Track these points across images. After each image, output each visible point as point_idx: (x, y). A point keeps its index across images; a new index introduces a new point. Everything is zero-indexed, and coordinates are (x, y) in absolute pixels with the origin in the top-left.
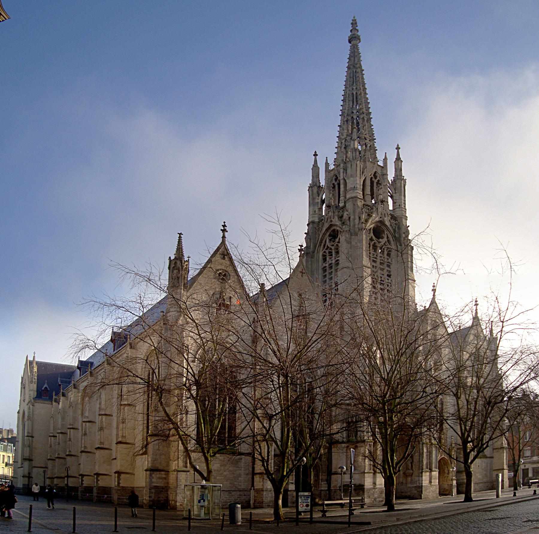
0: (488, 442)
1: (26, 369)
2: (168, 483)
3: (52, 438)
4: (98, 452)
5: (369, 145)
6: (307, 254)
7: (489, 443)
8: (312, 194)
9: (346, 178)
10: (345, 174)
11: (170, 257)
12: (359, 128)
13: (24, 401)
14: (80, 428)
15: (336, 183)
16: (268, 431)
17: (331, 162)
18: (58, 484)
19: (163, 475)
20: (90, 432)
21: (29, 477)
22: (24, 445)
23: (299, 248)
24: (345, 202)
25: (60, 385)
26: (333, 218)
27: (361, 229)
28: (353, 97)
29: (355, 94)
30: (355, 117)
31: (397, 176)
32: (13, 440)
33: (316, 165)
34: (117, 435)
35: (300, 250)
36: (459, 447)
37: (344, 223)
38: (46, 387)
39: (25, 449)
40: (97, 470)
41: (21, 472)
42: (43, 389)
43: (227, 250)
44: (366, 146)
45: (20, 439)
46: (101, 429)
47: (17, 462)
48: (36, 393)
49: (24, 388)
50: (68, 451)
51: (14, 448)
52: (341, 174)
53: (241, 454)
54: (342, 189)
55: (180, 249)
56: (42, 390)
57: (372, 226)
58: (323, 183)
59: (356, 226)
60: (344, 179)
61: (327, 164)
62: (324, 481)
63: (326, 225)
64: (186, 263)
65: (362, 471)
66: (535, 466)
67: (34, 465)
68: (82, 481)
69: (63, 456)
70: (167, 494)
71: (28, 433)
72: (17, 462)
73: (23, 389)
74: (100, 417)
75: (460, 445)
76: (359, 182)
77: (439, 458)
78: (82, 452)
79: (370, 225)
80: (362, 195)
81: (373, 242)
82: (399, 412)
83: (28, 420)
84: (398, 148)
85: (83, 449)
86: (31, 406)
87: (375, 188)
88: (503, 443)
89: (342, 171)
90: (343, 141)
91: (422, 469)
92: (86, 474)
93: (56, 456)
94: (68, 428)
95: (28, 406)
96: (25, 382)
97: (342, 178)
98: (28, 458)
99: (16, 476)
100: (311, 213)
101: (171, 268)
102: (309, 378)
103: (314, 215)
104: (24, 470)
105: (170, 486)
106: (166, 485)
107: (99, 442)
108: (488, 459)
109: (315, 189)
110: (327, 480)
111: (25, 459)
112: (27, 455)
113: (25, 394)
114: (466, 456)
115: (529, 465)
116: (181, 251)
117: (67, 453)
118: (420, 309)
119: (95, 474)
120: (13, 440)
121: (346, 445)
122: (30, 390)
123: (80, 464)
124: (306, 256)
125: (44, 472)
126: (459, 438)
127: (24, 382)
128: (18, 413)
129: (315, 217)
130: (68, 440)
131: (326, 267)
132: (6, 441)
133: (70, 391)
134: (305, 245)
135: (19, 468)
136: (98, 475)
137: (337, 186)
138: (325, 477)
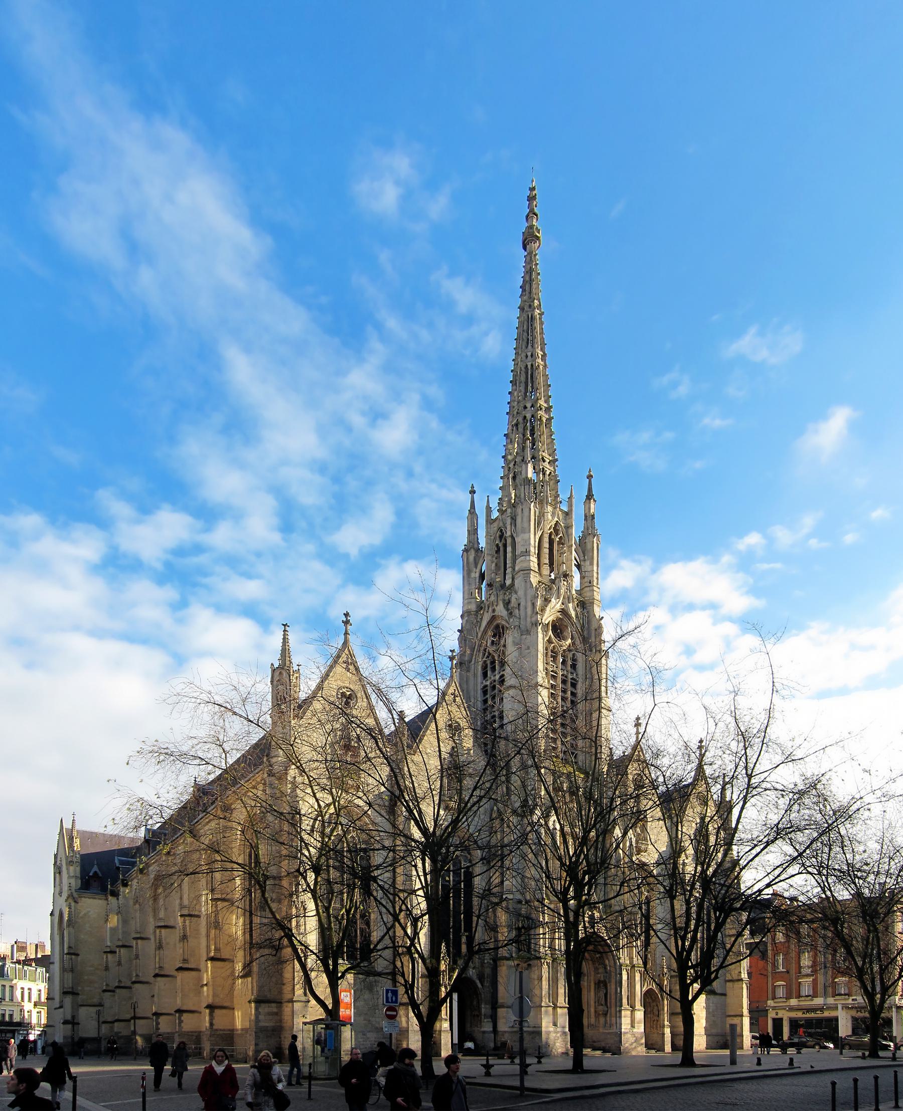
0: (717, 971)
1: (61, 842)
2: (281, 1021)
3: (109, 955)
4: (180, 976)
5: (548, 473)
6: (461, 664)
7: (720, 972)
8: (468, 563)
9: (515, 535)
10: (513, 527)
11: (272, 664)
12: (533, 439)
13: (60, 894)
14: (152, 937)
15: (500, 545)
16: (412, 941)
17: (494, 505)
18: (120, 1033)
19: (273, 1008)
20: (168, 944)
21: (72, 1022)
22: (63, 970)
23: (450, 654)
24: (513, 579)
25: (118, 868)
26: (497, 606)
27: (536, 624)
28: (527, 373)
29: (529, 367)
30: (528, 416)
31: (588, 529)
32: (43, 962)
33: (473, 510)
34: (208, 947)
35: (451, 659)
36: (675, 974)
37: (511, 613)
38: (96, 872)
39: (66, 976)
40: (179, 1003)
41: (60, 1015)
42: (91, 874)
43: (351, 655)
44: (544, 474)
45: (57, 959)
46: (184, 938)
47: (53, 999)
48: (79, 881)
49: (60, 873)
50: (134, 975)
51: (48, 975)
52: (509, 527)
53: (379, 974)
54: (509, 555)
55: (285, 652)
56: (90, 877)
57: (551, 619)
58: (483, 543)
59: (529, 619)
60: (512, 536)
61: (489, 510)
62: (487, 1018)
63: (486, 618)
64: (296, 675)
65: (538, 1004)
66: (794, 1015)
67: (80, 1003)
68: (158, 1024)
69: (129, 984)
70: (280, 1038)
71: (70, 947)
72: (53, 999)
73: (57, 875)
74: (183, 918)
75: (674, 971)
76: (533, 541)
77: (644, 989)
78: (180, 969)
79: (549, 615)
80: (536, 566)
81: (553, 645)
82: (295, 738)
83: (68, 925)
84: (590, 477)
85: (157, 971)
86: (73, 904)
87: (555, 552)
88: (740, 972)
89: (509, 521)
90: (511, 465)
91: (621, 1006)
92: (164, 1011)
93: (117, 984)
94: (134, 939)
95: (68, 903)
96: (61, 864)
97: (509, 533)
98: (70, 990)
99: (51, 1024)
100: (466, 597)
101: (275, 682)
102: (465, 861)
103: (470, 600)
104: (64, 1012)
105: (285, 1025)
106: (278, 1024)
107: (182, 959)
108: (718, 997)
109: (472, 554)
110: (491, 1017)
111: (65, 993)
112: (69, 984)
113: (61, 882)
114: (685, 989)
115: (783, 1011)
116: (287, 655)
117: (134, 979)
118: (618, 753)
119: (177, 1011)
120: (43, 962)
121: (516, 962)
122: (69, 877)
123: (153, 996)
124: (468, 616)
125: (99, 1013)
126: (673, 961)
127: (58, 862)
128: (52, 914)
129: (471, 602)
130: (133, 957)
131: (486, 686)
132: (34, 964)
133: (135, 878)
134: (457, 650)
135: (55, 1009)
136: (180, 1011)
137: (502, 549)
138: (489, 1012)
